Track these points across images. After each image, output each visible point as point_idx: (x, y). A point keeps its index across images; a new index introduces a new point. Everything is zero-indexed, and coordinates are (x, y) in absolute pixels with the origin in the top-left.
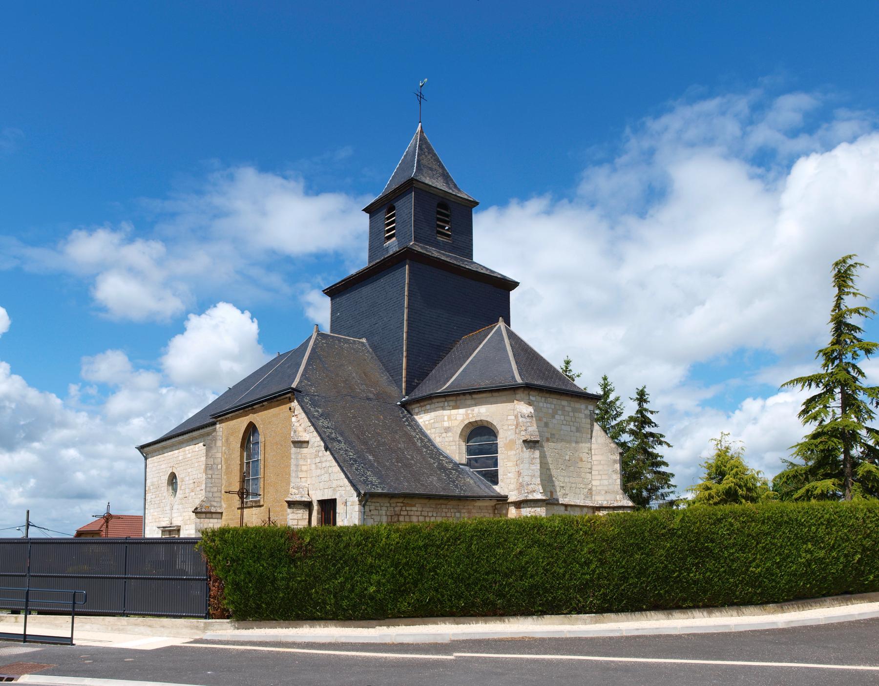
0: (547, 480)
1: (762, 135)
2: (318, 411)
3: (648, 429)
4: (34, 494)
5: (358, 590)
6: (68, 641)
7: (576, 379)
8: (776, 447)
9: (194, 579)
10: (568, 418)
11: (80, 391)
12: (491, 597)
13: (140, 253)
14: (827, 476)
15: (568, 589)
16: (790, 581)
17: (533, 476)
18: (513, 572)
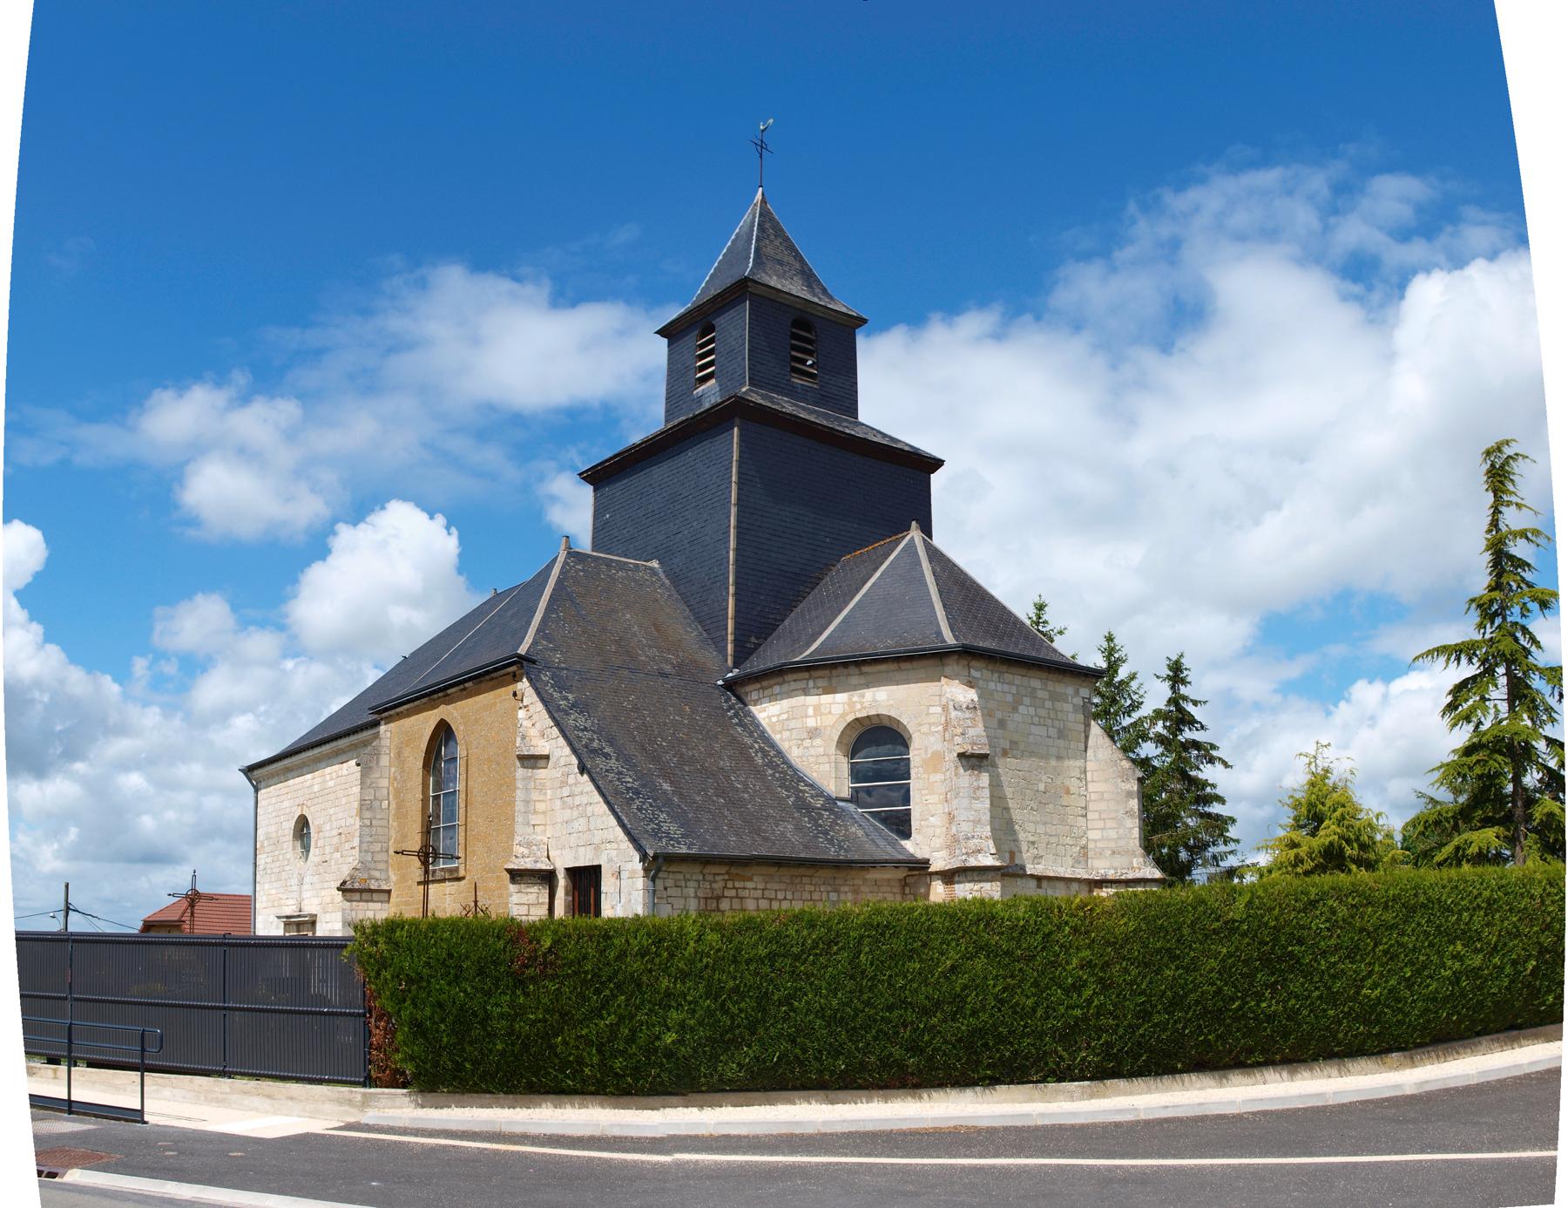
0: (1004, 829)
1: (1353, 233)
2: (566, 699)
3: (1188, 734)
4: (75, 854)
5: (642, 1038)
6: (136, 1116)
7: (1057, 638)
8: (1406, 771)
9: (341, 1014)
10: (1042, 712)
11: (149, 668)
12: (897, 1052)
13: (259, 421)
14: (1487, 822)
15: (1042, 1034)
16: (1427, 1010)
17: (977, 822)
18: (938, 1004)
